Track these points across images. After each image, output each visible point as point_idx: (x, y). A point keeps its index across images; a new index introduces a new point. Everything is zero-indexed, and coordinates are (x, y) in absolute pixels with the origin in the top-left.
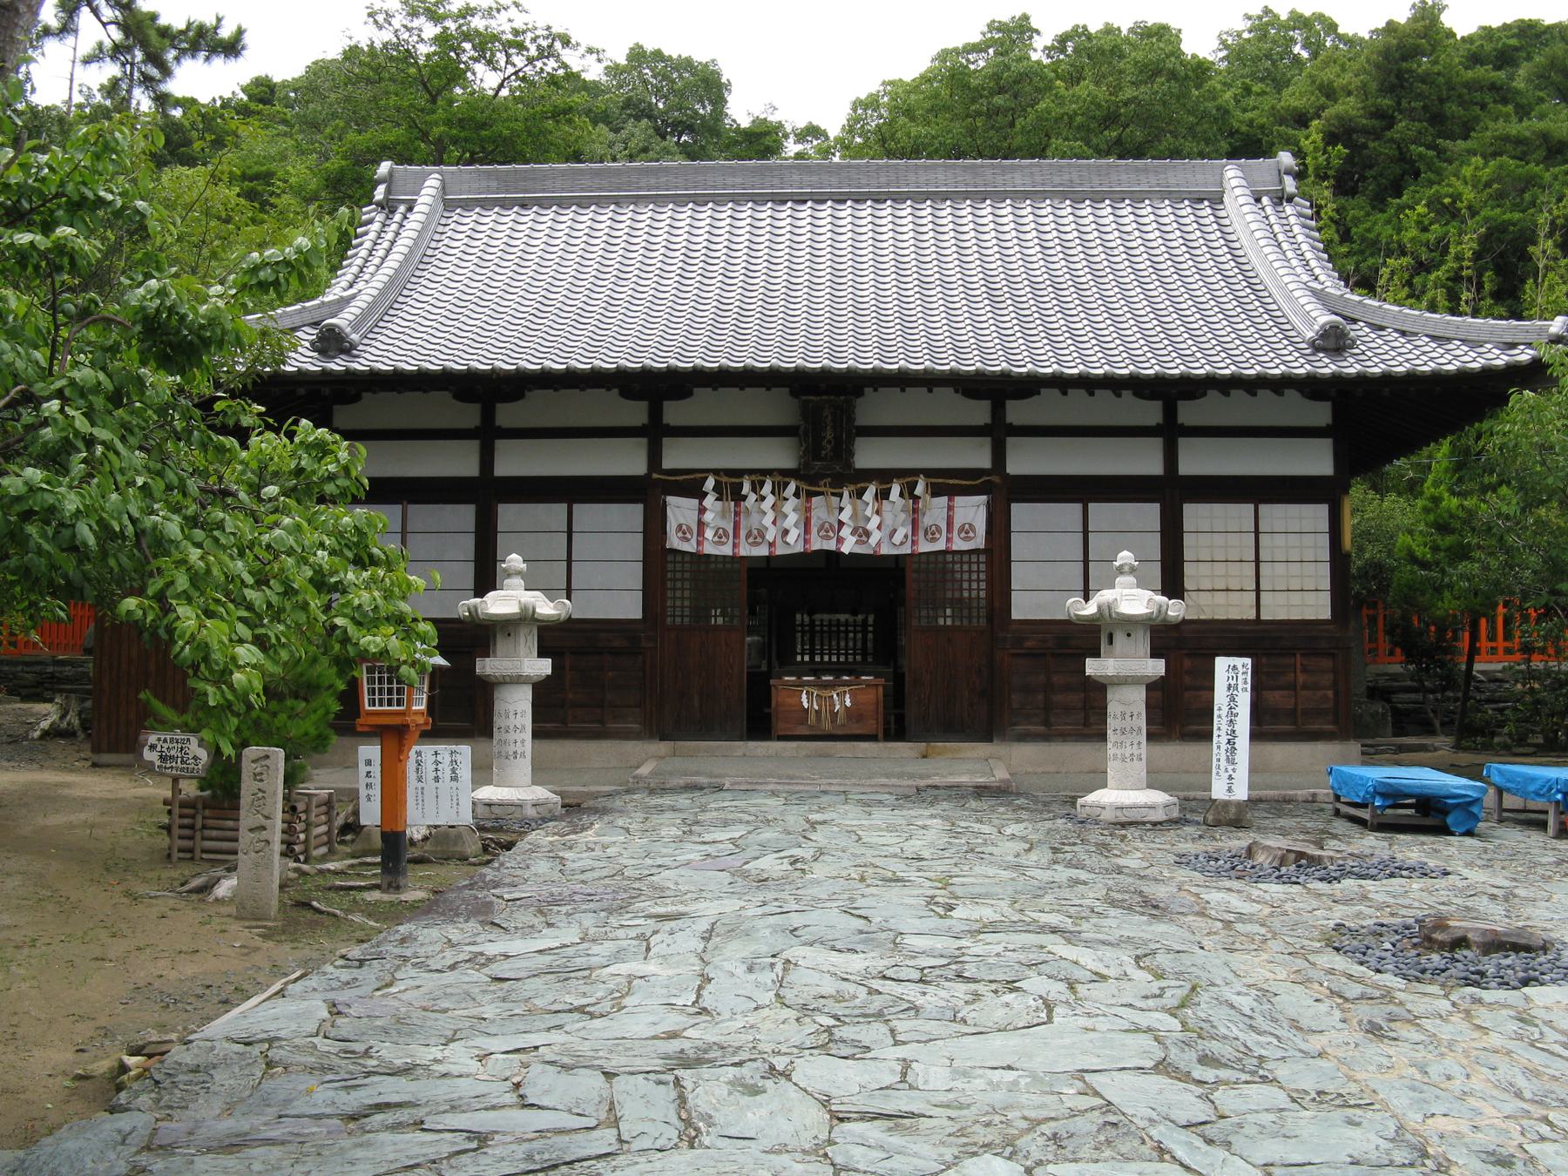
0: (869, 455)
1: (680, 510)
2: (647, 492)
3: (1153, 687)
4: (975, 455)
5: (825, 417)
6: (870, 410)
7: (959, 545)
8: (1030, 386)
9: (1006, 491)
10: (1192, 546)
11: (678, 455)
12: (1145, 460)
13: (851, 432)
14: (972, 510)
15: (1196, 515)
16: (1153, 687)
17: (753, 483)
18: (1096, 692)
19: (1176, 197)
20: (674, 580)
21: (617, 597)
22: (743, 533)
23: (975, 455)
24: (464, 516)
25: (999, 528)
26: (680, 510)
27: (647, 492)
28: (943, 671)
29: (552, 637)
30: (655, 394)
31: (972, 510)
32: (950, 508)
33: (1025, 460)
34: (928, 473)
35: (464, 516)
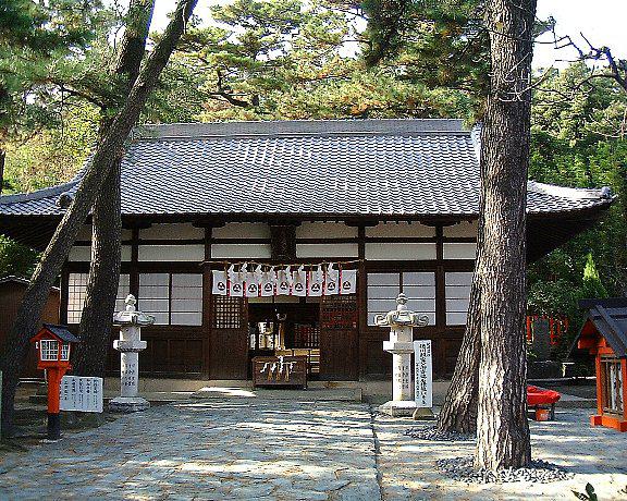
0: (303, 251)
1: (218, 276)
2: (204, 269)
3: (142, 354)
4: (351, 251)
5: (282, 234)
6: (303, 231)
7: (343, 292)
8: (372, 220)
9: (365, 268)
10: (449, 293)
11: (219, 252)
12: (427, 252)
13: (293, 242)
14: (350, 276)
15: (143, 278)
16: (142, 354)
17: (322, 266)
18: (388, 357)
19: (449, 135)
20: (220, 304)
21: (189, 314)
22: (310, 286)
23: (351, 251)
24: (429, 277)
25: (362, 284)
26: (218, 276)
27: (204, 269)
28: (342, 353)
29: (149, 332)
30: (207, 225)
31: (350, 276)
32: (401, 276)
33: (374, 253)
34: (332, 260)
35: (429, 277)
